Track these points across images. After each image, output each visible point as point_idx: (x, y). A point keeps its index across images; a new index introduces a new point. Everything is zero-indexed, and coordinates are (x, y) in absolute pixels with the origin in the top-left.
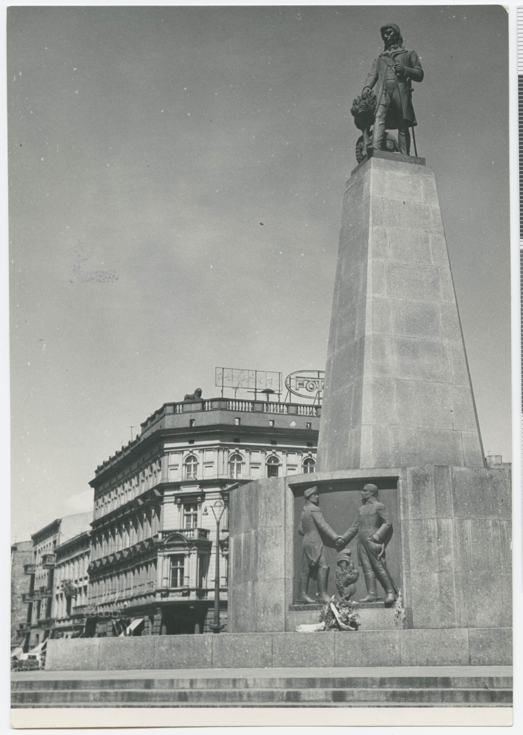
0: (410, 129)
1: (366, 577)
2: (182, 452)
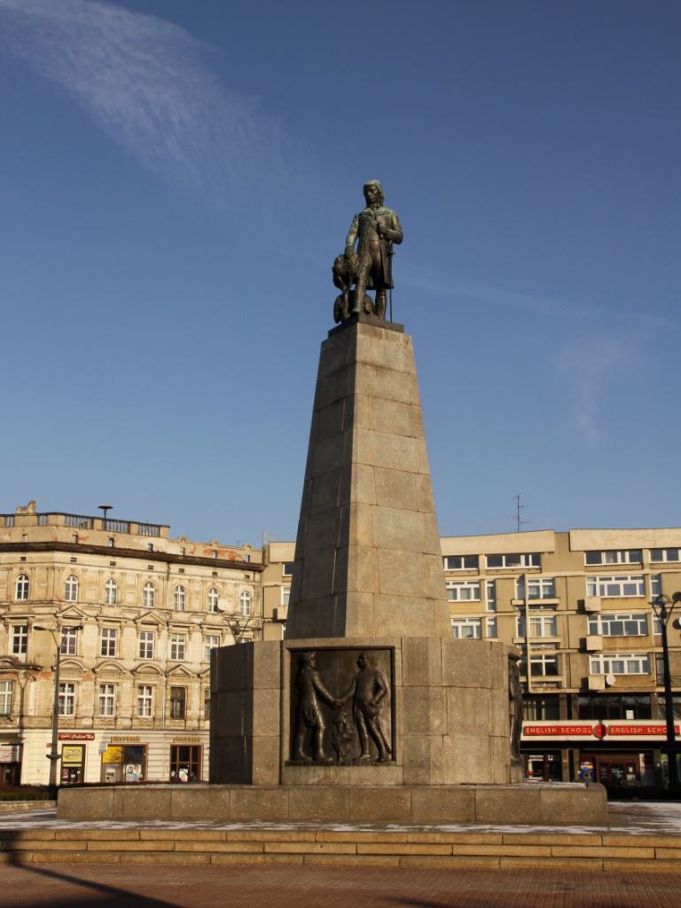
1: (362, 740)
2: (11, 569)
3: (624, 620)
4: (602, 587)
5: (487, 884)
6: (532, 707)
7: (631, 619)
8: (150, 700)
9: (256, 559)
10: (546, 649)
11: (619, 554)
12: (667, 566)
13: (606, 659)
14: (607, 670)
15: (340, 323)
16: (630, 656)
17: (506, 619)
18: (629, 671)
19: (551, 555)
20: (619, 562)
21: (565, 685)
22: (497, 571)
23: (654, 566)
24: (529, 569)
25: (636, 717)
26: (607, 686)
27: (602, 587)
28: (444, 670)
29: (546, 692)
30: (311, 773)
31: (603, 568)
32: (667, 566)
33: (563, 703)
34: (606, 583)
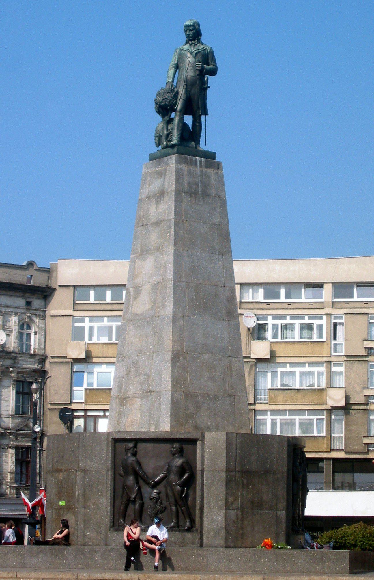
0: (203, 117)
9: (39, 280)
22: (347, 303)
28: (238, 459)
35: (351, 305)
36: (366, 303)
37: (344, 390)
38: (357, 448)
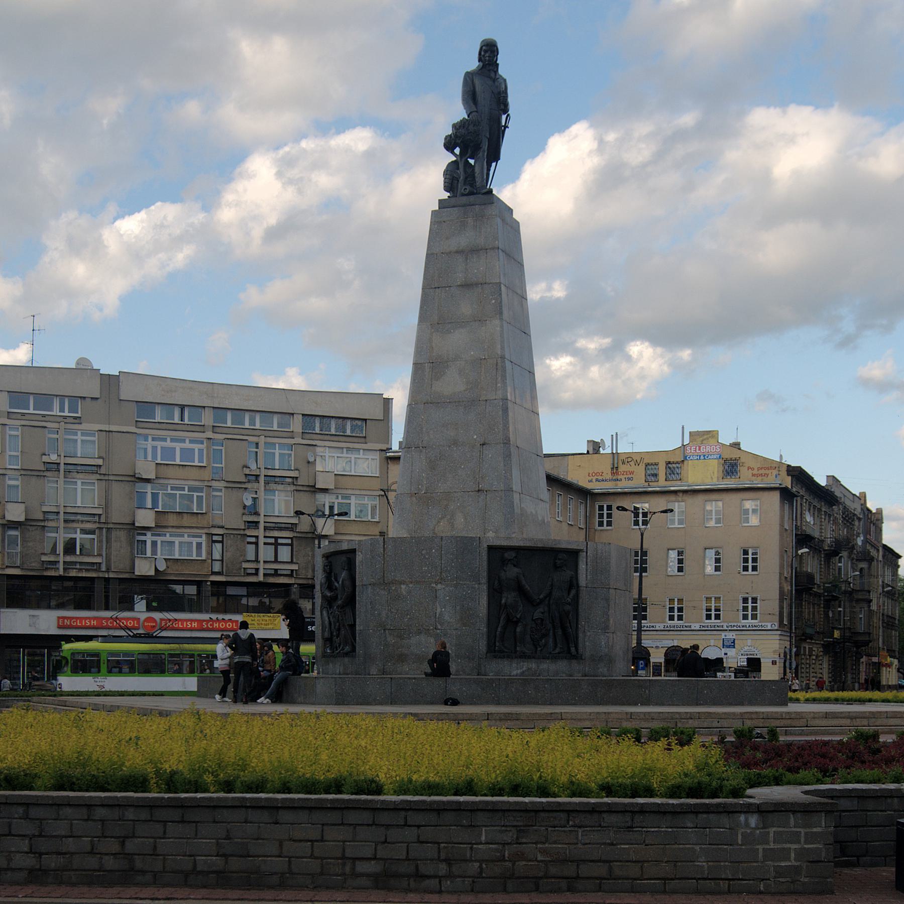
3: (178, 492)
4: (154, 448)
5: (583, 775)
6: (819, 605)
7: (186, 492)
8: (256, 574)
10: (82, 521)
11: (177, 412)
12: (231, 431)
13: (155, 538)
14: (154, 552)
15: (457, 151)
16: (183, 536)
17: (34, 479)
18: (180, 555)
19: (94, 402)
20: (177, 420)
21: (104, 568)
23: (217, 430)
24: (65, 417)
25: (149, 608)
26: (156, 570)
27: (154, 448)
29: (80, 575)
30: (514, 665)
31: (157, 426)
32: (231, 431)
33: (99, 587)
34: (159, 444)
35: (27, 417)
36: (44, 416)
37: (23, 506)
38: (35, 565)
